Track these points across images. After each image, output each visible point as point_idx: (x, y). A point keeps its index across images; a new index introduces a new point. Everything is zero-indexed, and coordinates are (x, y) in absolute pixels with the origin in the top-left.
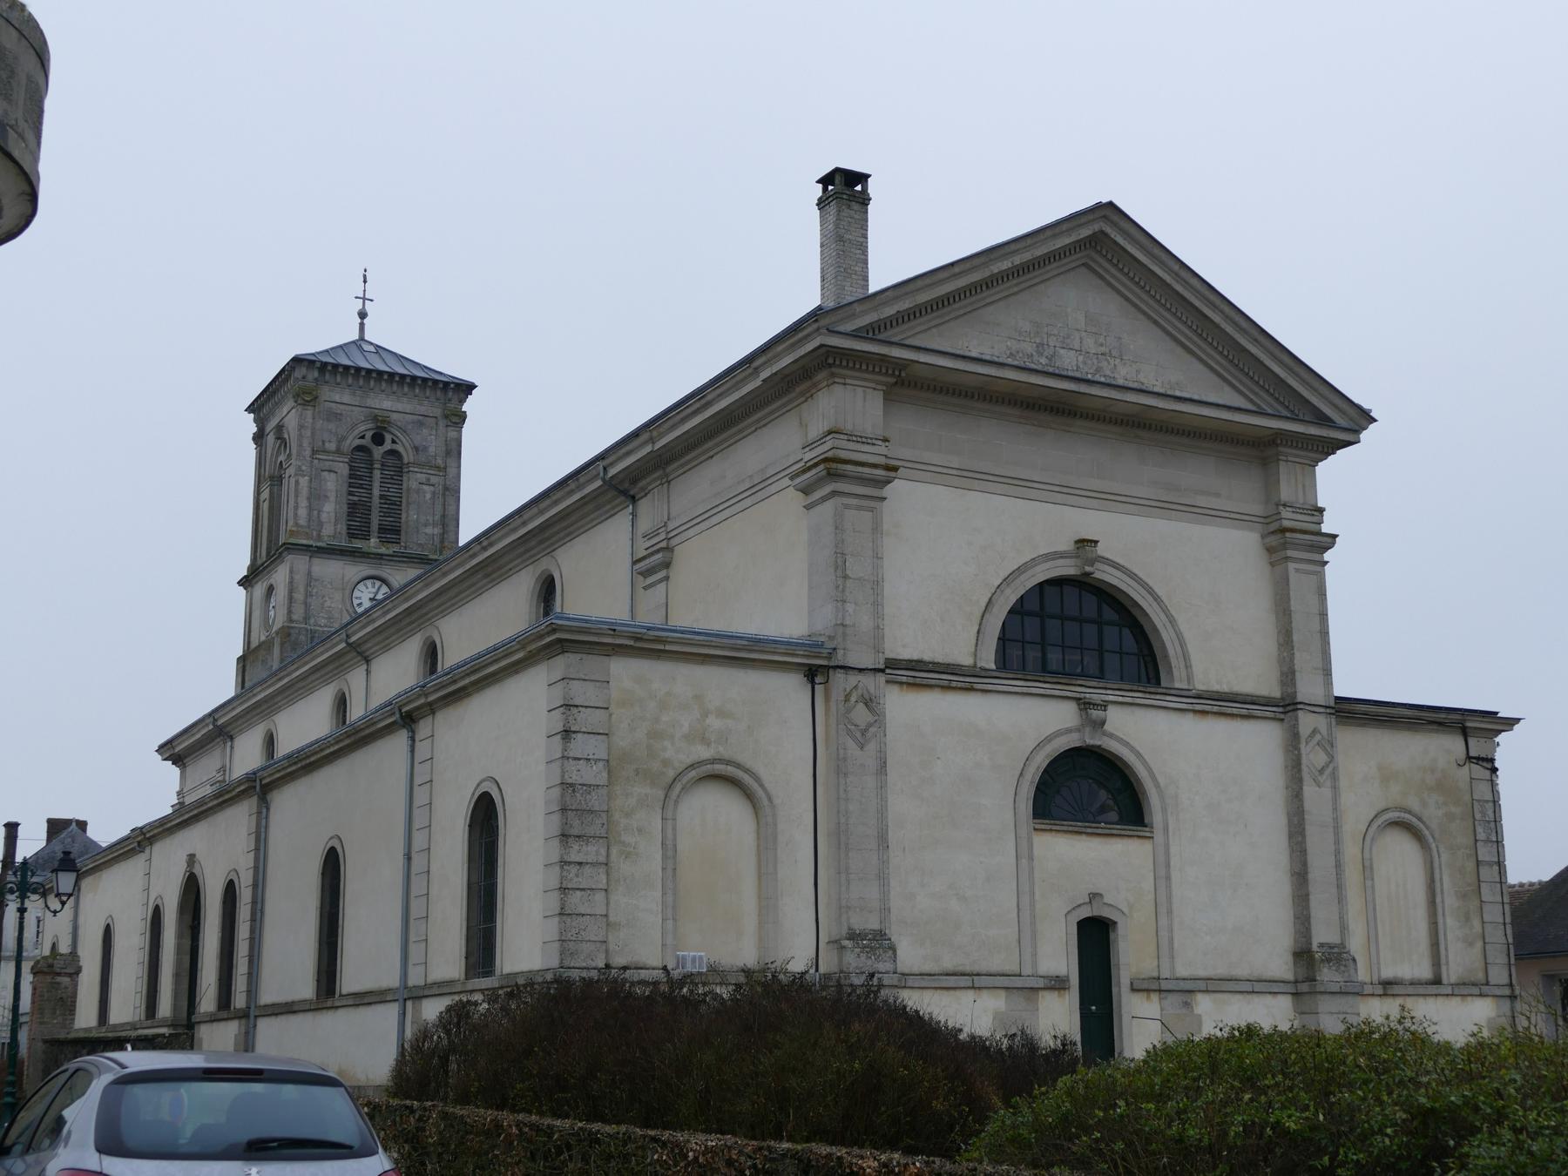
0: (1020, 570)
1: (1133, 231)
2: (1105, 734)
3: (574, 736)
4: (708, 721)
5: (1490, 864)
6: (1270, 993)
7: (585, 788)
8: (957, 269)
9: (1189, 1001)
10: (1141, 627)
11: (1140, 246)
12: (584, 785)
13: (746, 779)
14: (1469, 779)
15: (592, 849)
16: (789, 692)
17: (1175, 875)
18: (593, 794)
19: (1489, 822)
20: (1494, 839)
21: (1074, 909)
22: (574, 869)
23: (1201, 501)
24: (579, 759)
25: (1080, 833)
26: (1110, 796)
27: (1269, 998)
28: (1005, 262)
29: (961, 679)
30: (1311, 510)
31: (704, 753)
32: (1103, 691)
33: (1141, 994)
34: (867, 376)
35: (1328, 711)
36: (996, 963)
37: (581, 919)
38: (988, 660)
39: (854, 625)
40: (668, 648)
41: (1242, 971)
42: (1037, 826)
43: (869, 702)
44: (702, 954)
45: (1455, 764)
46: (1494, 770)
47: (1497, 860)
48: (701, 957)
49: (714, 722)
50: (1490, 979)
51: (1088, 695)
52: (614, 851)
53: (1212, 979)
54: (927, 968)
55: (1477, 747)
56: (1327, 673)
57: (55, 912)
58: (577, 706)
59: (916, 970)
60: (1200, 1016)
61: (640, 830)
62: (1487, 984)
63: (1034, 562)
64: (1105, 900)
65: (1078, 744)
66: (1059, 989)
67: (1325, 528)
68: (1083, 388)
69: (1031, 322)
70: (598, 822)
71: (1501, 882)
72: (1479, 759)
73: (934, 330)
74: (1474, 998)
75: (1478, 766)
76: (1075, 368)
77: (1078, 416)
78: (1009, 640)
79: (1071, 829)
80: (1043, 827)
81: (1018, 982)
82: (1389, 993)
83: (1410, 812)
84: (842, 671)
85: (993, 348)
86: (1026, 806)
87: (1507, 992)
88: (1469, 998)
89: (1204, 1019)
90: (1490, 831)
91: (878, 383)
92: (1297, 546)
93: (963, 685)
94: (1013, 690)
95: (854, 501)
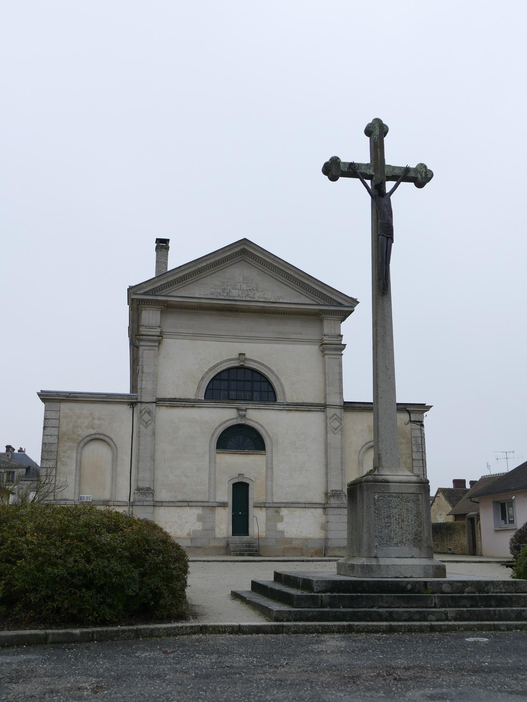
0: (215, 366)
2: (247, 419)
4: (94, 422)
5: (418, 460)
6: (313, 508)
8: (183, 268)
10: (271, 384)
13: (107, 439)
16: (125, 411)
17: (275, 468)
18: (52, 446)
19: (419, 444)
20: (421, 451)
23: (292, 336)
24: (48, 435)
26: (251, 441)
27: (313, 510)
28: (204, 263)
29: (190, 403)
31: (92, 432)
33: (258, 508)
35: (341, 407)
39: (145, 388)
41: (302, 500)
42: (217, 452)
43: (149, 413)
45: (404, 424)
47: (422, 458)
48: (89, 497)
49: (96, 422)
52: (59, 464)
54: (172, 500)
55: (414, 417)
56: (341, 394)
58: (48, 419)
59: (167, 500)
61: (68, 457)
63: (221, 363)
64: (245, 476)
65: (236, 423)
66: (224, 507)
67: (343, 343)
68: (233, 303)
69: (221, 282)
70: (54, 455)
73: (182, 289)
76: (238, 296)
77: (287, 314)
79: (231, 452)
81: (207, 504)
85: (205, 292)
86: (214, 445)
89: (284, 517)
91: (158, 308)
92: (329, 349)
93: (190, 405)
95: (148, 348)
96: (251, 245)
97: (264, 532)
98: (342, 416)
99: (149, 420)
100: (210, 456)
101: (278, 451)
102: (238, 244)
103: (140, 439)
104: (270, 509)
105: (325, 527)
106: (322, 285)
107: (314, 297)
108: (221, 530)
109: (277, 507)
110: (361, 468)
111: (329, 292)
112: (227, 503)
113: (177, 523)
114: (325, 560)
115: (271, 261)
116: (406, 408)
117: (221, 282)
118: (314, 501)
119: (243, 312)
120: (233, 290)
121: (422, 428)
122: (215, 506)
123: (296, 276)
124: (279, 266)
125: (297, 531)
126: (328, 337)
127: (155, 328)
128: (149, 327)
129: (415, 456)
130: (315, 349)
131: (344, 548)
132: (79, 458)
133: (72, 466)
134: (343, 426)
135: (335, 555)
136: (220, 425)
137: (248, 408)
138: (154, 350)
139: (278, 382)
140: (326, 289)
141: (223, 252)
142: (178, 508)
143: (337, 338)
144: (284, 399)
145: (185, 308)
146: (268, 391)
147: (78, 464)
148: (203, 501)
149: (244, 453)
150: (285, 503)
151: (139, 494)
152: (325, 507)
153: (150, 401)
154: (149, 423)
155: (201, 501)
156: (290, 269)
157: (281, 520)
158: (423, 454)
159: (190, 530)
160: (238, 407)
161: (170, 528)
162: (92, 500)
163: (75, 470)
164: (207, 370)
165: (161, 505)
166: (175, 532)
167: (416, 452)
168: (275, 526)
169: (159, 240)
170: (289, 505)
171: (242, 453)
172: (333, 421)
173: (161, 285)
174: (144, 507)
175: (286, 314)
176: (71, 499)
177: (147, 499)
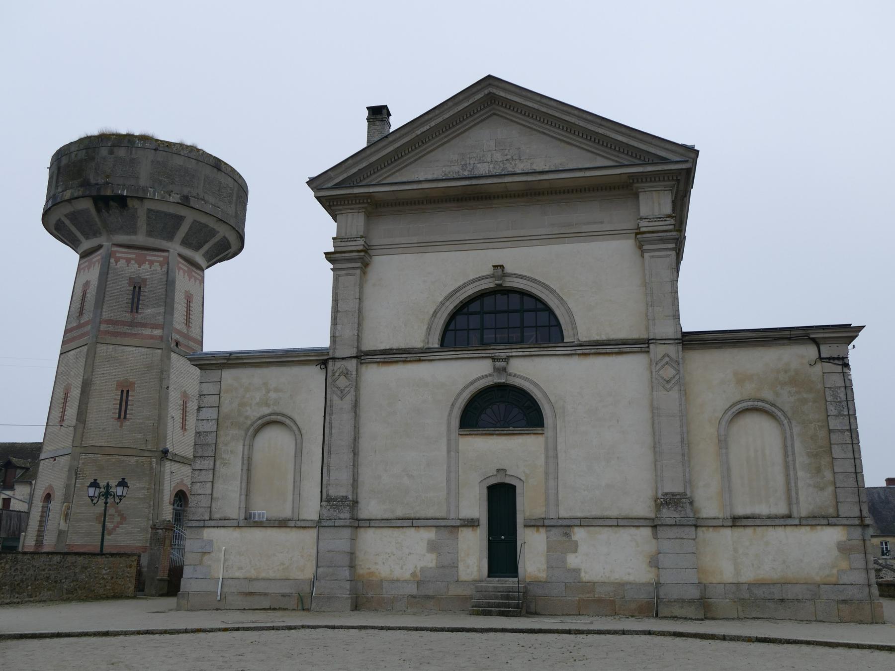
1: (507, 87)
2: (511, 375)
3: (202, 409)
5: (842, 431)
6: (633, 526)
7: (205, 433)
9: (568, 532)
11: (515, 93)
12: (205, 432)
14: (822, 374)
15: (206, 462)
16: (314, 377)
19: (840, 402)
20: (846, 413)
21: (485, 479)
22: (197, 473)
23: (585, 228)
24: (203, 420)
25: (493, 434)
27: (633, 530)
29: (415, 355)
30: (663, 218)
31: (266, 411)
32: (510, 351)
33: (532, 529)
34: (352, 206)
35: (676, 341)
36: (431, 513)
37: (199, 496)
38: (435, 343)
39: (341, 336)
40: (245, 361)
41: (614, 513)
42: (461, 433)
44: (265, 512)
45: (809, 366)
46: (847, 365)
47: (848, 428)
50: (840, 513)
51: (497, 354)
52: (218, 463)
53: (587, 518)
54: (386, 516)
55: (826, 351)
56: (677, 317)
57: (118, 503)
58: (205, 395)
59: (379, 517)
60: (577, 541)
62: (838, 516)
63: (465, 285)
64: (508, 473)
66: (473, 526)
68: (474, 182)
69: (459, 154)
71: (852, 444)
72: (830, 359)
73: (397, 174)
74: (824, 527)
75: (830, 364)
78: (468, 327)
79: (484, 432)
80: (465, 433)
81: (443, 523)
82: (737, 524)
83: (762, 401)
84: (332, 360)
86: (456, 422)
87: (857, 522)
88: (819, 528)
89: (579, 544)
90: (841, 408)
92: (650, 242)
93: (414, 359)
94: (446, 358)
95: (343, 272)
96: (501, 85)
97: (543, 571)
98: (680, 357)
99: (347, 387)
100: (449, 440)
101: (565, 427)
102: (479, 87)
103: (333, 417)
104: (554, 530)
105: (654, 562)
106: (628, 132)
107: (618, 157)
108: (468, 567)
109: (566, 526)
110: (724, 451)
111: (641, 141)
112: (478, 520)
113: (394, 555)
114: (615, 631)
115: (536, 106)
116: (808, 333)
117: (459, 154)
118: (635, 514)
119: (498, 197)
120: (479, 165)
121: (846, 370)
122: (458, 527)
123: (582, 123)
124: (550, 112)
125: (604, 569)
126: (647, 220)
127: (355, 239)
128: (346, 240)
129: (834, 424)
130: (627, 245)
131: (689, 602)
132: (246, 453)
133: (236, 466)
134: (681, 375)
135: (673, 615)
136: (466, 387)
137: (512, 356)
138: (354, 274)
139: (563, 308)
140: (635, 138)
141: (456, 104)
142: (397, 529)
143: (665, 220)
144: (574, 336)
145: (403, 204)
146: (550, 326)
147: (246, 462)
148: (437, 517)
149: (505, 432)
150: (580, 518)
151: (329, 507)
152: (655, 525)
153: (349, 356)
154: (346, 392)
155: (434, 518)
156: (569, 114)
157: (574, 548)
158: (852, 420)
159: (416, 567)
160: (493, 355)
161: (384, 563)
162: (267, 518)
163: (240, 473)
164: (443, 298)
165: (368, 525)
166: (391, 570)
167: (836, 416)
168: (564, 561)
169: (371, 109)
170: (587, 522)
171: (502, 432)
172: (663, 367)
173: (359, 170)
174: (336, 528)
175: (572, 192)
176: (234, 518)
177: (342, 516)
